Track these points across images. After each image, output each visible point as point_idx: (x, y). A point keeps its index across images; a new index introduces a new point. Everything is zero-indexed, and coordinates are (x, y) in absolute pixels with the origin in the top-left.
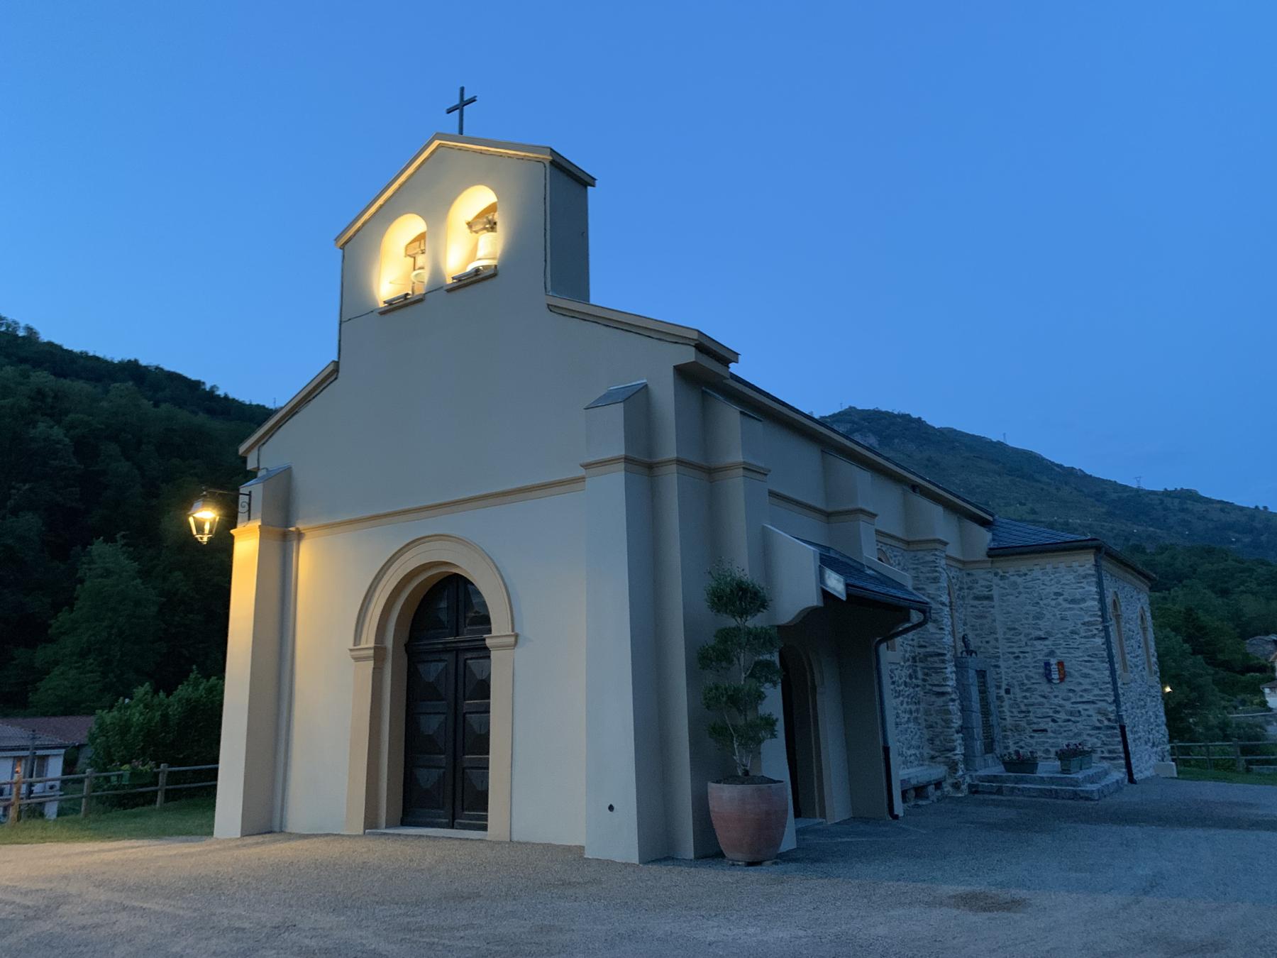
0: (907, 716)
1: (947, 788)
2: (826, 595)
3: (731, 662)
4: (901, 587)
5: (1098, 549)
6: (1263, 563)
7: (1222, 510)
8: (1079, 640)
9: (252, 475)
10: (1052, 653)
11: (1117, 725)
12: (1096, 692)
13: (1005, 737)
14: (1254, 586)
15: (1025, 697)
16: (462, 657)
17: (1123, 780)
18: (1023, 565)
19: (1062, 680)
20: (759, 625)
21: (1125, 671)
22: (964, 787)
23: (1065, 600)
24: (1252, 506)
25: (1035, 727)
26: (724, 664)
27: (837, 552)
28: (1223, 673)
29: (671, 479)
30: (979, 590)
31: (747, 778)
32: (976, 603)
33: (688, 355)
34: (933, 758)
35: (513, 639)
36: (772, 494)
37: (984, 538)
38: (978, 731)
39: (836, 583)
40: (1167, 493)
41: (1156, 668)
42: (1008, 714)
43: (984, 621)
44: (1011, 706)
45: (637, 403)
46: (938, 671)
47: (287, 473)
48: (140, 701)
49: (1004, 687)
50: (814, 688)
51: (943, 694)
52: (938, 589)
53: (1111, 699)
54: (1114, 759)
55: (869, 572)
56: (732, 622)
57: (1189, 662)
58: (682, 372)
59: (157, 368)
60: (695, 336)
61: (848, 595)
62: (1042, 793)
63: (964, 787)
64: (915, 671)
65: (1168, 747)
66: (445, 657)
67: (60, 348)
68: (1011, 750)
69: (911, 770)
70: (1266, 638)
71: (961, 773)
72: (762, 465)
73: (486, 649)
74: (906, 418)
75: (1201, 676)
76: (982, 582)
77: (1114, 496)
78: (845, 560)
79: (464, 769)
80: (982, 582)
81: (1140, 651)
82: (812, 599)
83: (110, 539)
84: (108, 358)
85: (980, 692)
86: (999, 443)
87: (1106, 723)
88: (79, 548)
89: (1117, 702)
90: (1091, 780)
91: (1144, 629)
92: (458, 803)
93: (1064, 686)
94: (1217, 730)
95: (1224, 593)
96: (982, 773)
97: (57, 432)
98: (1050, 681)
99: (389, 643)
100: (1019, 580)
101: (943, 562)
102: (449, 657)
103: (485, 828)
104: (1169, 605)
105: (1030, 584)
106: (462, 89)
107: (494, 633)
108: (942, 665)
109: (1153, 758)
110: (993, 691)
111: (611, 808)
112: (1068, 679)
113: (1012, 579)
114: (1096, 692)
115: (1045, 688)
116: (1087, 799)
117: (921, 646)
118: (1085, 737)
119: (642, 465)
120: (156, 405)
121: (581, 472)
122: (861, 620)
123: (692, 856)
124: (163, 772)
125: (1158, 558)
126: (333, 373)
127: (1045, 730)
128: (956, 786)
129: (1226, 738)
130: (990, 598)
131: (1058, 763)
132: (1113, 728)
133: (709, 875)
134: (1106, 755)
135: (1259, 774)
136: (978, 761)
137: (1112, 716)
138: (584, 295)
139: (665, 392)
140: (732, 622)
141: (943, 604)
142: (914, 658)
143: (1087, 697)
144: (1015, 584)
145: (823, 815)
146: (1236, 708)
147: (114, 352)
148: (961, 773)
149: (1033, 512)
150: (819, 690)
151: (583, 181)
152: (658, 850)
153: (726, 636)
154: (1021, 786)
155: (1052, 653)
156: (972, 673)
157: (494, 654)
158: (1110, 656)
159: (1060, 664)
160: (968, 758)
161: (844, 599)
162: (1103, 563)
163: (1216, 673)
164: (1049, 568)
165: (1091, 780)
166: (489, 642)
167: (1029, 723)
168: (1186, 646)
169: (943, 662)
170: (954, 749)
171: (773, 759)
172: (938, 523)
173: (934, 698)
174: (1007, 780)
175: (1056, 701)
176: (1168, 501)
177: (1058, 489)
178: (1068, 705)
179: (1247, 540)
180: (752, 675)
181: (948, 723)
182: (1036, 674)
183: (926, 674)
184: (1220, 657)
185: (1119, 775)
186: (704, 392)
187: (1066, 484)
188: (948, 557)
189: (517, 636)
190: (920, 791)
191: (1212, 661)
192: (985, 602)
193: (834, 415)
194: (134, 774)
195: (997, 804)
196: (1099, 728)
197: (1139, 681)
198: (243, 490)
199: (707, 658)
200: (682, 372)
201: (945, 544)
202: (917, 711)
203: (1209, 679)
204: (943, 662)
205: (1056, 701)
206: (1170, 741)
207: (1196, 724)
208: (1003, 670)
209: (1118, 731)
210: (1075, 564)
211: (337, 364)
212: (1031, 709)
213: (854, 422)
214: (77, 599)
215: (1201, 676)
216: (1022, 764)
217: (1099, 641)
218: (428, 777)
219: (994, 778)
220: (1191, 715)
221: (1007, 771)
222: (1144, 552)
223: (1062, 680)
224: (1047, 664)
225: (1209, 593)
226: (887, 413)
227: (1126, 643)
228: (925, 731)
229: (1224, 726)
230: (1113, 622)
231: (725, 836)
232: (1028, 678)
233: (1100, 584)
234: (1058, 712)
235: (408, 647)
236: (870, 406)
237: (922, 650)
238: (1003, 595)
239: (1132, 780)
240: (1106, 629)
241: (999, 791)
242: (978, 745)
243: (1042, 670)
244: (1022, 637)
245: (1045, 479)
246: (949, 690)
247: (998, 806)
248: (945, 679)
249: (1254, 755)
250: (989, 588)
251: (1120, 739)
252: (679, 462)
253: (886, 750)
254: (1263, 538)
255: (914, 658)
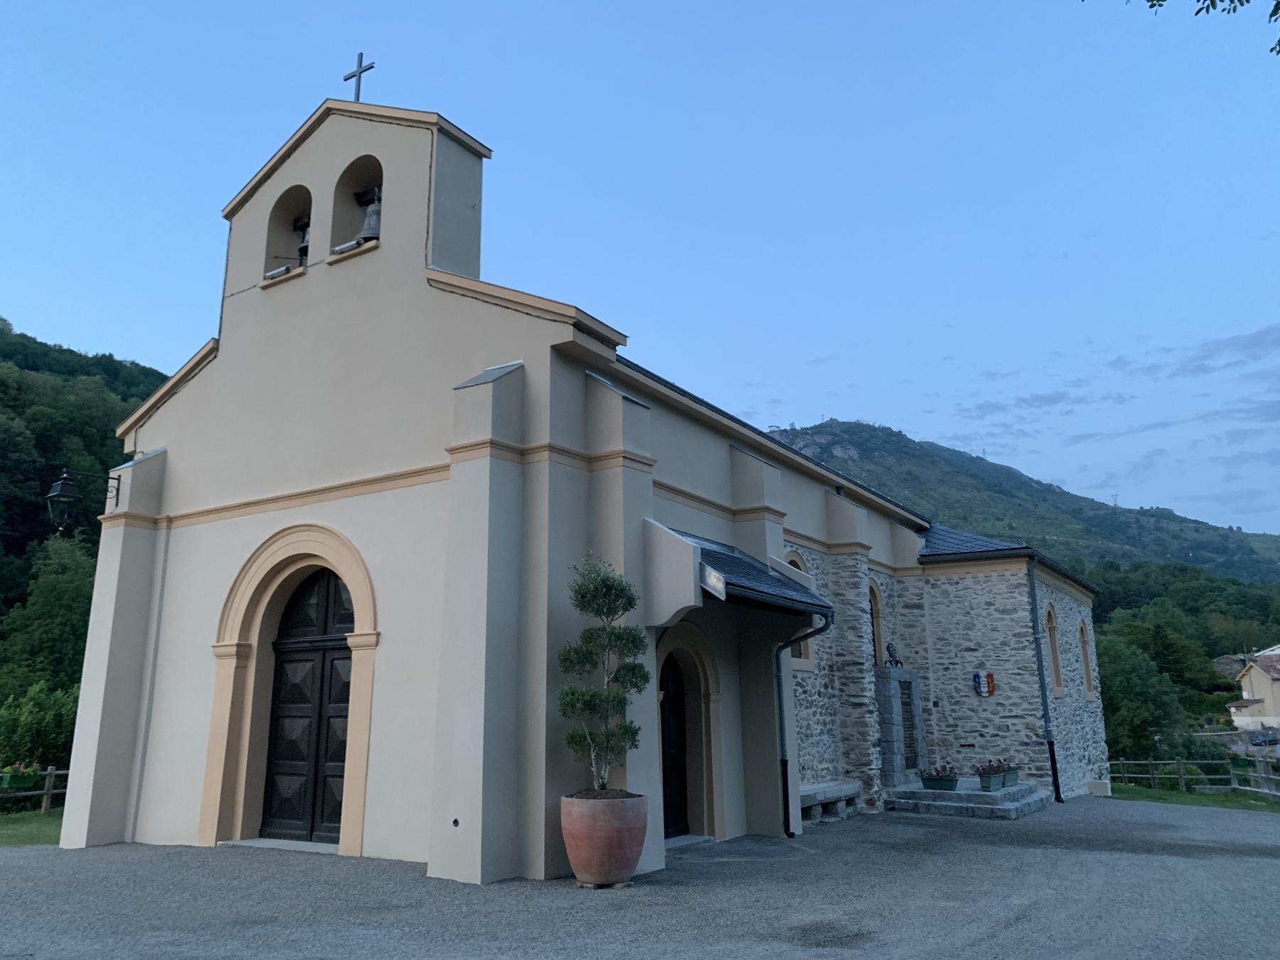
0: (819, 727)
1: (861, 804)
2: (706, 595)
3: (595, 665)
4: (804, 590)
5: (1031, 557)
6: (1234, 583)
7: (1197, 530)
8: (1009, 652)
9: (130, 457)
10: (981, 665)
11: (1045, 741)
12: (1025, 705)
13: (933, 752)
14: (1222, 604)
15: (953, 711)
16: (329, 656)
17: (1048, 798)
18: (956, 572)
19: (991, 693)
20: (632, 625)
21: (1059, 684)
22: (880, 804)
23: (997, 610)
24: (1226, 527)
25: (963, 741)
26: (588, 667)
27: (741, 552)
28: (1190, 692)
29: (543, 466)
30: (910, 598)
31: (604, 791)
32: (906, 611)
33: (566, 334)
34: (848, 772)
35: (373, 639)
36: (657, 484)
37: (917, 544)
38: (899, 746)
39: (716, 582)
40: (1142, 512)
41: (1096, 683)
42: (936, 727)
43: (913, 630)
44: (939, 720)
45: (511, 385)
46: (857, 681)
47: (162, 457)
48: (32, 699)
49: (933, 699)
50: (708, 695)
51: (861, 705)
52: (858, 595)
53: (1040, 714)
54: (1041, 776)
55: (772, 573)
56: (598, 622)
57: (1154, 680)
58: (561, 353)
59: (133, 363)
60: (573, 313)
61: (727, 594)
62: (960, 811)
63: (880, 804)
64: (832, 681)
65: (1108, 765)
66: (310, 656)
67: (34, 341)
68: (938, 766)
69: (822, 785)
70: (1234, 657)
71: (876, 789)
72: (648, 455)
73: (348, 649)
74: (887, 432)
75: (1166, 693)
76: (912, 590)
77: (1091, 513)
78: (751, 561)
79: (325, 777)
80: (912, 590)
81: (1078, 665)
82: (689, 598)
83: (68, 534)
84: (83, 352)
85: (904, 703)
86: (978, 458)
87: (1034, 738)
88: (35, 543)
89: (1045, 716)
90: (1012, 797)
91: (1084, 643)
92: (318, 813)
93: (993, 700)
94: (1181, 749)
95: (1194, 611)
96: (901, 788)
97: (18, 424)
98: (979, 694)
99: (254, 640)
100: (951, 588)
101: (865, 567)
102: (317, 656)
103: (336, 841)
104: (1138, 623)
105: (961, 593)
106: (361, 55)
107: (357, 631)
108: (860, 675)
109: (1088, 775)
110: (918, 704)
111: (456, 822)
112: (996, 693)
113: (944, 587)
114: (1025, 705)
115: (973, 701)
116: (1003, 818)
117: (838, 655)
118: (1012, 753)
119: (512, 451)
120: (124, 399)
121: (446, 459)
122: (752, 624)
123: (541, 876)
124: (50, 775)
125: (1132, 576)
126: (213, 350)
127: (973, 746)
128: (871, 803)
129: (1190, 756)
130: (920, 607)
131: (978, 779)
132: (1042, 744)
133: (560, 898)
134: (1034, 772)
135: (1202, 794)
136: (898, 777)
137: (1041, 732)
138: (474, 272)
139: (541, 372)
140: (598, 622)
141: (863, 611)
142: (831, 667)
143: (1016, 712)
144: (946, 593)
145: (712, 833)
146: (1202, 726)
147: (89, 347)
148: (876, 789)
149: (1011, 528)
150: (713, 697)
151: (478, 153)
152: (504, 868)
153: (589, 636)
154: (938, 803)
155: (981, 665)
156: (894, 685)
157: (355, 655)
158: (1040, 668)
159: (990, 676)
160: (886, 775)
161: (723, 597)
162: (1036, 572)
163: (1183, 691)
164: (981, 576)
165: (1012, 797)
166: (350, 642)
167: (957, 738)
168: (1153, 663)
169: (861, 671)
170: (869, 763)
171: (644, 773)
172: (863, 527)
173: (850, 710)
174: (925, 797)
175: (984, 715)
176: (1143, 520)
177: (1036, 506)
178: (997, 720)
179: (1222, 559)
180: (616, 679)
181: (864, 735)
182: (965, 686)
183: (843, 684)
184: (1187, 675)
185: (1046, 792)
186: (588, 375)
187: (1045, 500)
188: (871, 561)
189: (378, 635)
190: (828, 807)
191: (1178, 678)
192: (916, 611)
193: (815, 427)
194: (15, 777)
195: (908, 822)
196: (1027, 744)
197: (1075, 696)
198: (113, 474)
199: (573, 659)
200: (561, 353)
201: (868, 548)
202: (833, 722)
203: (1175, 696)
204: (861, 671)
205: (984, 715)
206: (1110, 759)
207: (1160, 741)
208: (932, 681)
209: (1046, 747)
210: (1008, 573)
211: (217, 341)
212: (959, 722)
213: (835, 435)
214: (30, 595)
215: (1166, 693)
216: (942, 781)
217: (1030, 653)
218: (289, 785)
219: (912, 795)
220: (1156, 733)
221: (926, 787)
222: (1117, 568)
223: (991, 693)
224: (976, 677)
225: (1178, 611)
226: (868, 426)
227: (1060, 657)
228: (841, 744)
229: (1189, 744)
230: (1047, 634)
231: (577, 854)
232: (957, 690)
233: (1032, 595)
234: (986, 726)
235: (277, 647)
236: (851, 418)
237: (840, 659)
238: (934, 604)
239: (1058, 799)
240: (1037, 641)
241: (915, 809)
242: (899, 760)
243: (971, 683)
244: (952, 648)
245: (1022, 494)
246: (866, 701)
247: (908, 824)
248: (863, 690)
249: (1219, 773)
250: (920, 596)
251: (1048, 755)
252: (551, 448)
253: (784, 763)
254: (1236, 558)
255: (831, 667)
